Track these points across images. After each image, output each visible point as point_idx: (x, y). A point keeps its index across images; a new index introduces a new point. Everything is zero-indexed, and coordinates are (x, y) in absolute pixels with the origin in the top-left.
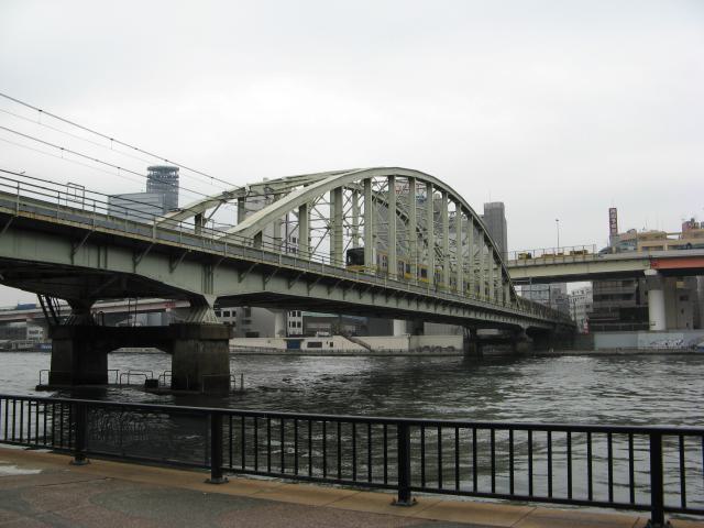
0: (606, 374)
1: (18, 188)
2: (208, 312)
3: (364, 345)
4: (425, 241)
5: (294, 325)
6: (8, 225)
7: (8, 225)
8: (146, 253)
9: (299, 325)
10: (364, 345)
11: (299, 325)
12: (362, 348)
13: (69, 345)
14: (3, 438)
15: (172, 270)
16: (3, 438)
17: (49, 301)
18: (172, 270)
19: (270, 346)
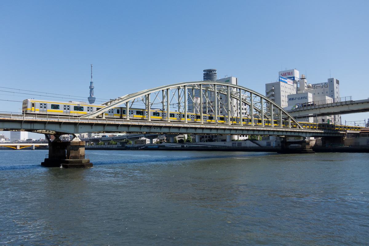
3: (257, 144)
10: (257, 144)
12: (257, 146)
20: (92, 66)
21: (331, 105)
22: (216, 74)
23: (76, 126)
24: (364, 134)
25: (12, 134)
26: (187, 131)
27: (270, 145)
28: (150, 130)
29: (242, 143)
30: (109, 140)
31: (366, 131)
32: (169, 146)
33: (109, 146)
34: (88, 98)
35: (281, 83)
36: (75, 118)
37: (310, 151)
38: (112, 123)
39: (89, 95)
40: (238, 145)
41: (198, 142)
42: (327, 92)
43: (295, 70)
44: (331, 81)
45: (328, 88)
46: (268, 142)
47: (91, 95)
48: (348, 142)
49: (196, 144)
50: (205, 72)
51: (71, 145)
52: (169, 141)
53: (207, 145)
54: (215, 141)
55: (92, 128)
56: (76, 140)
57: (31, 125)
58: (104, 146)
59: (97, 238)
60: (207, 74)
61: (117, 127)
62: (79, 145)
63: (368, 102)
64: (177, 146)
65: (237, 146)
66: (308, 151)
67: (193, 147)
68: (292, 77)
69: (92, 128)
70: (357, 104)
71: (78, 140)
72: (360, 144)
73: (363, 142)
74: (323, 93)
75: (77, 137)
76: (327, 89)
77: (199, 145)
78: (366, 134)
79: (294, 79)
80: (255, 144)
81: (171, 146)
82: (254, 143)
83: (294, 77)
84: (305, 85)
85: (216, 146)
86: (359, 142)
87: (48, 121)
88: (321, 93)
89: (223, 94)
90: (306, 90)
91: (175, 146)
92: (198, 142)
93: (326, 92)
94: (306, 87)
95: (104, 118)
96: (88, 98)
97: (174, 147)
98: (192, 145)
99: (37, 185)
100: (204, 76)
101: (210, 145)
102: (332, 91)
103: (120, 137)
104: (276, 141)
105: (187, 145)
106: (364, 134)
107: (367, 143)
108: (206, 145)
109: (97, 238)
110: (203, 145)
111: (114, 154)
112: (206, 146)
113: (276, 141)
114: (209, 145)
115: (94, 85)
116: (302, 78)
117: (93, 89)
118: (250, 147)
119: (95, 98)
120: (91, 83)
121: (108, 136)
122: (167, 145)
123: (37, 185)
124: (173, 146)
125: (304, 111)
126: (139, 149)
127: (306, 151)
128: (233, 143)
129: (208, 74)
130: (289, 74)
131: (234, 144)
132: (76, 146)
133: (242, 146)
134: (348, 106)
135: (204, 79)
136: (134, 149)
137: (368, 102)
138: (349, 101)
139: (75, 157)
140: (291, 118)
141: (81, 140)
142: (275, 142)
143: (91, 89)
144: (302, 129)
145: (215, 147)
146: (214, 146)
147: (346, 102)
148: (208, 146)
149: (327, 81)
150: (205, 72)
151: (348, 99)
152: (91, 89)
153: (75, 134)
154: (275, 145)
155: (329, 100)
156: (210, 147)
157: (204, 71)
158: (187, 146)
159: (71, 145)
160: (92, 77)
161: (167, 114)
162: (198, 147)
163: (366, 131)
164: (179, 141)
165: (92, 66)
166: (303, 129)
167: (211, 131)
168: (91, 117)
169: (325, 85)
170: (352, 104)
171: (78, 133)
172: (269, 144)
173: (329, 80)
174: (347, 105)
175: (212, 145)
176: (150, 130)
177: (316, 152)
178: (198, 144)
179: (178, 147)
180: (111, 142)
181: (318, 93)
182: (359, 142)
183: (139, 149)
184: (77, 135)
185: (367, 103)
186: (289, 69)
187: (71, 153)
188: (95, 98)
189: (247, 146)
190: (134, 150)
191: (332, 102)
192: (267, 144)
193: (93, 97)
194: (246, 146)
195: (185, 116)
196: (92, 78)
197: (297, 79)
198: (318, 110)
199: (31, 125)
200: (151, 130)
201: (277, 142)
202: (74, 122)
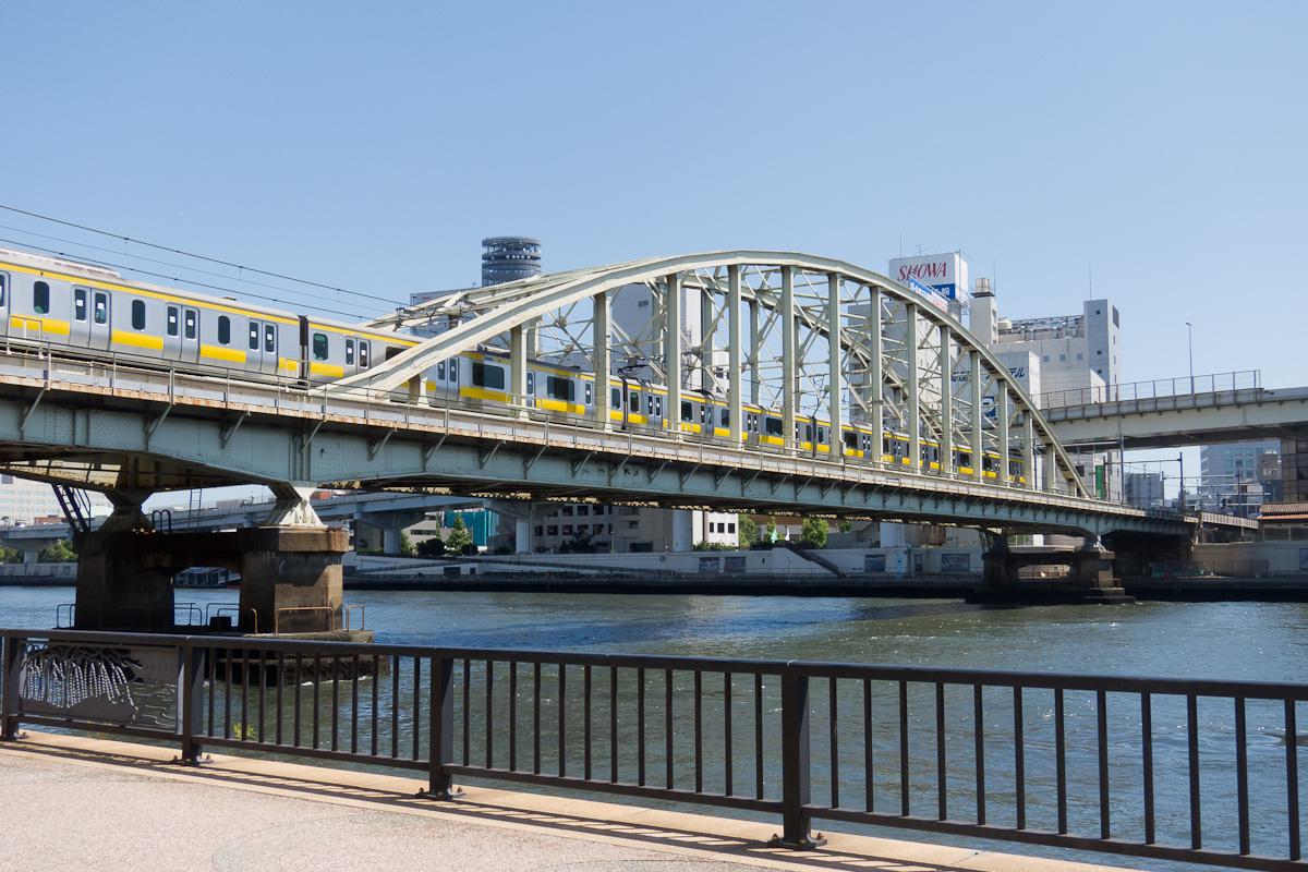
0: (528, 616)
1: (367, 395)
2: (298, 509)
3: (824, 564)
4: (905, 398)
5: (721, 528)
6: (165, 415)
7: (165, 415)
8: (438, 446)
9: (731, 528)
10: (824, 564)
11: (731, 528)
12: (825, 571)
13: (101, 563)
14: (1301, 707)
15: (223, 443)
16: (1301, 707)
17: (71, 496)
18: (223, 443)
19: (663, 566)
21: (1170, 405)
22: (537, 262)
23: (297, 439)
24: (1275, 526)
26: (743, 489)
27: (882, 570)
28: (610, 477)
29: (747, 561)
30: (45, 540)
31: (1278, 517)
32: (380, 569)
33: (45, 569)
35: (945, 310)
36: (295, 394)
37: (1116, 593)
38: (466, 434)
40: (726, 569)
41: (528, 553)
42: (1080, 357)
43: (957, 257)
44: (1097, 310)
45: (1086, 338)
46: (875, 556)
48: (1209, 560)
49: (519, 563)
50: (491, 250)
51: (282, 547)
52: (366, 546)
53: (578, 567)
54: (604, 547)
55: (371, 456)
56: (300, 524)
57: (74, 415)
58: (19, 570)
60: (497, 258)
61: (476, 456)
62: (324, 548)
63: (1303, 400)
64: (426, 571)
65: (721, 571)
66: (1109, 593)
67: (506, 574)
68: (945, 286)
69: (371, 456)
70: (1281, 402)
71: (309, 524)
72: (1272, 568)
73: (1283, 559)
74: (1063, 358)
75: (304, 504)
76: (1082, 345)
77: (534, 564)
78: (1284, 526)
79: (952, 296)
80: (813, 564)
81: (386, 569)
82: (808, 558)
83: (952, 287)
84: (994, 323)
85: (622, 569)
86: (1267, 561)
87: (176, 401)
88: (1059, 358)
90: (995, 342)
91: (414, 572)
92: (528, 553)
93: (1075, 356)
94: (994, 328)
95: (423, 403)
97: (408, 576)
98: (498, 565)
100: (484, 266)
101: (591, 568)
102: (1099, 353)
104: (908, 552)
105: (475, 565)
106: (1275, 526)
107: (1302, 562)
108: (573, 566)
110: (554, 565)
111: (1220, 618)
112: (570, 570)
113: (908, 552)
114: (585, 567)
116: (979, 291)
118: (795, 577)
121: (32, 522)
122: (367, 566)
124: (404, 572)
125: (1085, 422)
126: (222, 580)
127: (1102, 593)
128: (702, 559)
129: (505, 258)
130: (932, 270)
131: (709, 563)
132: (307, 554)
133: (747, 572)
134: (1241, 409)
135: (484, 278)
136: (190, 583)
137: (1303, 400)
138: (1247, 391)
139: (301, 621)
140: (1057, 451)
141: (323, 519)
142: (905, 558)
144: (1086, 501)
145: (616, 575)
146: (611, 569)
147: (1236, 393)
148: (581, 571)
149: (1079, 311)
150: (491, 250)
151: (1245, 383)
153: (296, 489)
154: (904, 571)
155: (1097, 390)
157: (486, 243)
158: (473, 570)
159: (282, 547)
161: (665, 401)
162: (532, 574)
163: (1278, 517)
164: (421, 546)
166: (1087, 498)
167: (823, 496)
168: (358, 395)
169: (1072, 327)
170: (1260, 403)
171: (307, 479)
172: (876, 564)
173: (1089, 305)
174: (1239, 405)
175: (601, 568)
176: (610, 477)
177: (1139, 599)
178: (525, 564)
179: (432, 576)
180: (51, 549)
181: (1080, 357)
182: (1267, 561)
183: (222, 580)
184: (305, 492)
185: (1298, 404)
186: (932, 249)
187: (278, 597)
189: (775, 571)
190: (557, 591)
191: (1104, 400)
192: (866, 561)
194: (766, 571)
195: (732, 420)
197: (962, 294)
198: (1113, 422)
199: (74, 415)
200: (685, 486)
201: (912, 556)
202: (300, 415)
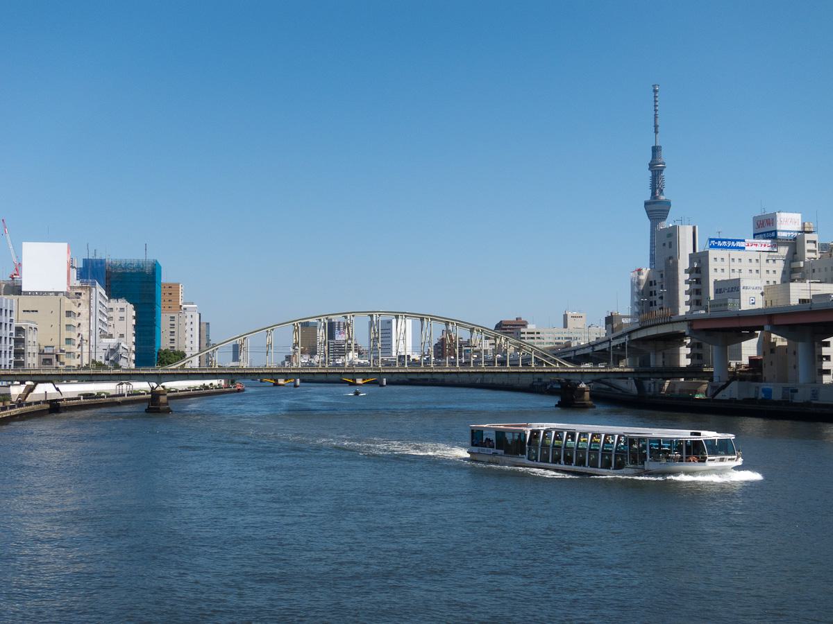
20: (655, 91)
25: (388, 331)
34: (646, 204)
39: (649, 192)
47: (654, 194)
59: (180, 588)
89: (330, 373)
96: (646, 204)
99: (748, 527)
103: (812, 312)
109: (180, 588)
115: (664, 156)
117: (661, 170)
119: (668, 203)
120: (656, 150)
123: (748, 527)
143: (656, 171)
152: (656, 171)
156: (605, 389)
160: (659, 129)
165: (655, 91)
188: (668, 203)
193: (662, 198)
196: (656, 132)
